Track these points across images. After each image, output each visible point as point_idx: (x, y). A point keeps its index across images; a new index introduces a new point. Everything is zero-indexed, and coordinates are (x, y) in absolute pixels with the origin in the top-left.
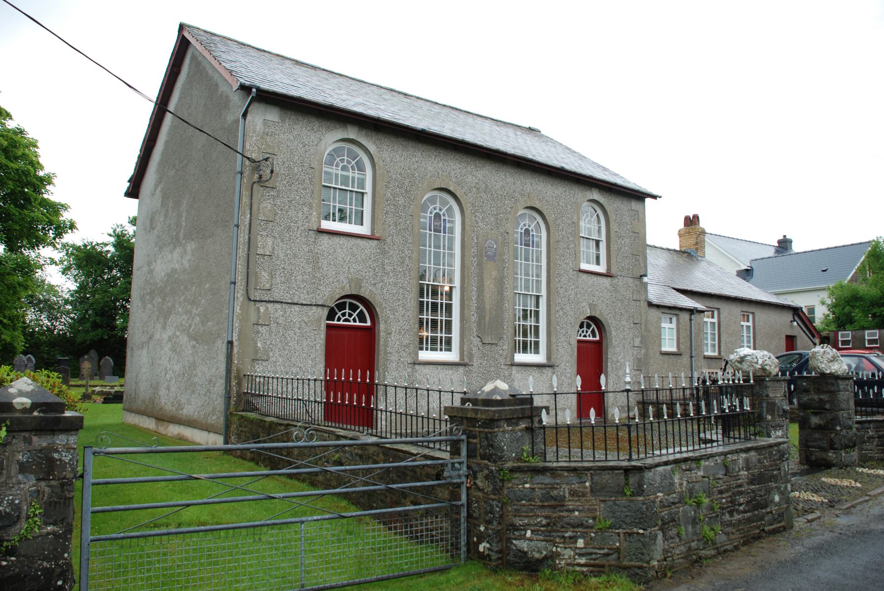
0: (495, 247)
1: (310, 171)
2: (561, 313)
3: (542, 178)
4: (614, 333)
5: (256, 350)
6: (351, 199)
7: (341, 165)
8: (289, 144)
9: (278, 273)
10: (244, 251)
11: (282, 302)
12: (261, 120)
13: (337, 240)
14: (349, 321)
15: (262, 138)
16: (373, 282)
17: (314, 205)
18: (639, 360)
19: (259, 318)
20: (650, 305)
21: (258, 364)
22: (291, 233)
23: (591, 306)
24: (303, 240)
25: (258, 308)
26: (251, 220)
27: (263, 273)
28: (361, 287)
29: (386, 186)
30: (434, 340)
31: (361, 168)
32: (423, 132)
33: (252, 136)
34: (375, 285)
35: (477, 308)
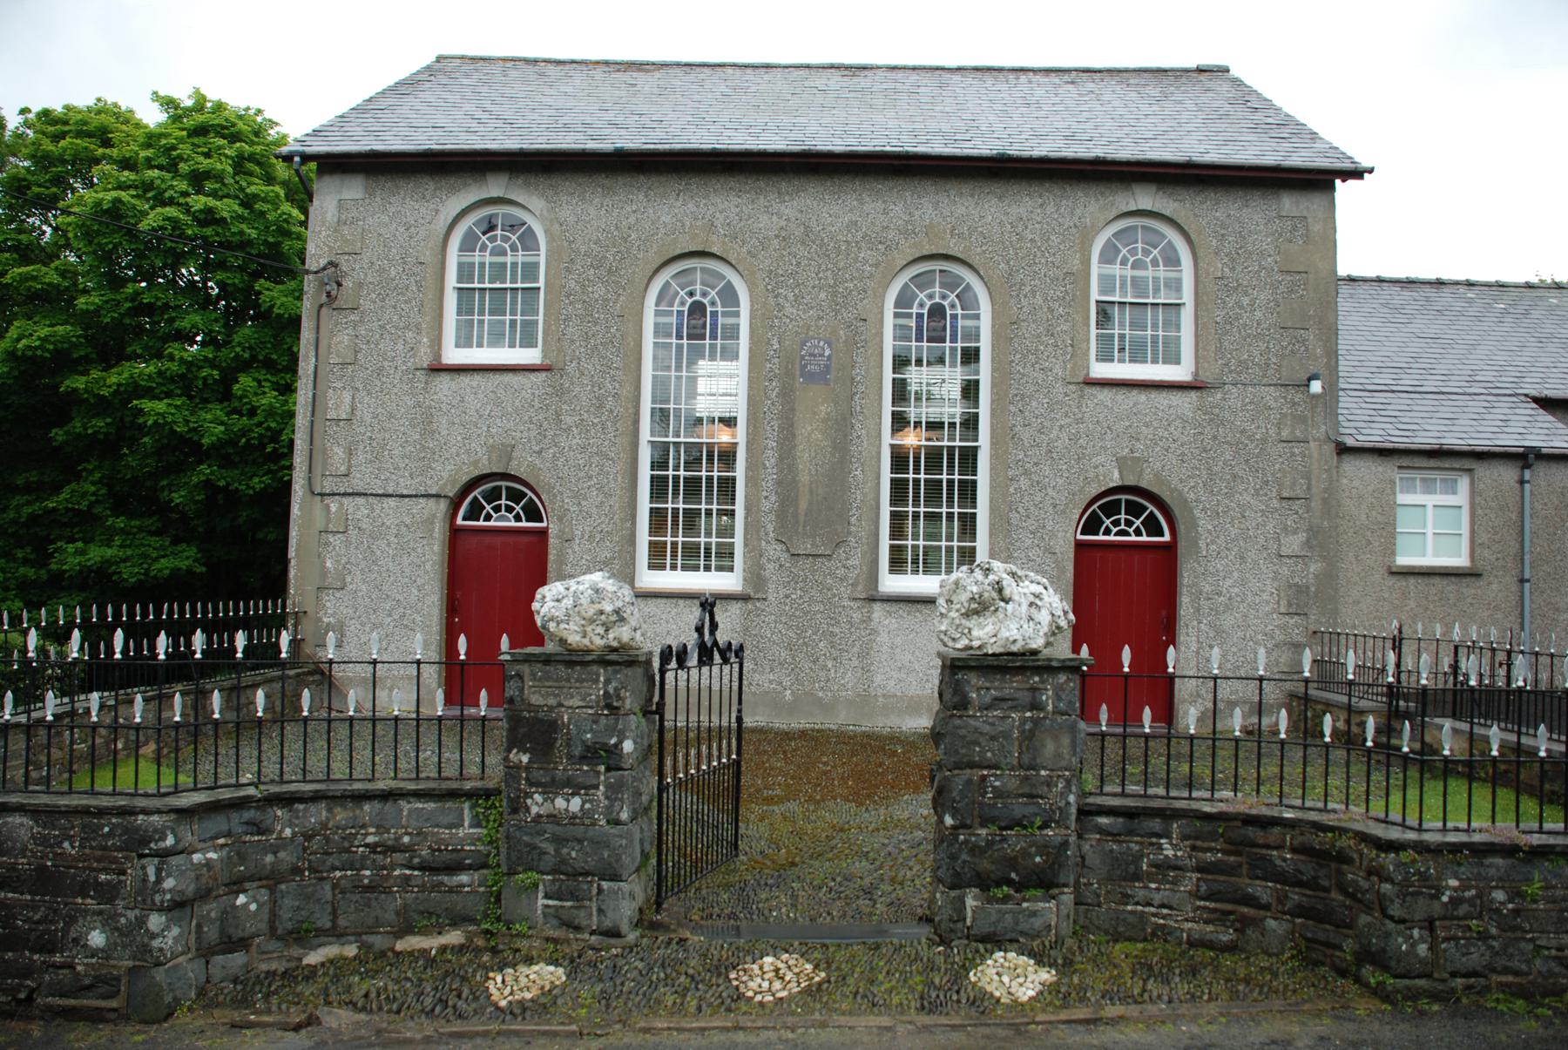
0: (827, 353)
1: (417, 270)
2: (1024, 483)
3: (966, 188)
4: (1204, 524)
5: (324, 572)
6: (514, 302)
7: (1132, 260)
8: (382, 231)
9: (361, 447)
10: (305, 417)
11: (366, 494)
12: (335, 203)
13: (465, 380)
14: (1126, 534)
15: (336, 231)
16: (537, 449)
17: (424, 326)
18: (1301, 590)
19: (328, 520)
20: (1343, 450)
21: (328, 595)
22: (384, 379)
23: (1121, 463)
24: (405, 387)
25: (328, 506)
26: (316, 367)
27: (336, 449)
28: (510, 459)
29: (568, 270)
30: (691, 551)
31: (1172, 261)
32: (1098, 162)
33: (320, 232)
34: (540, 452)
35: (779, 483)
